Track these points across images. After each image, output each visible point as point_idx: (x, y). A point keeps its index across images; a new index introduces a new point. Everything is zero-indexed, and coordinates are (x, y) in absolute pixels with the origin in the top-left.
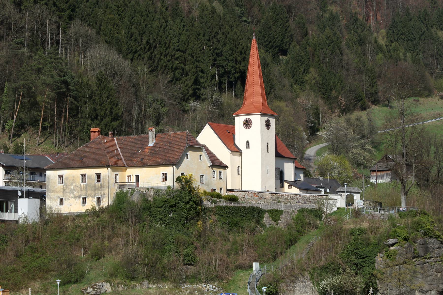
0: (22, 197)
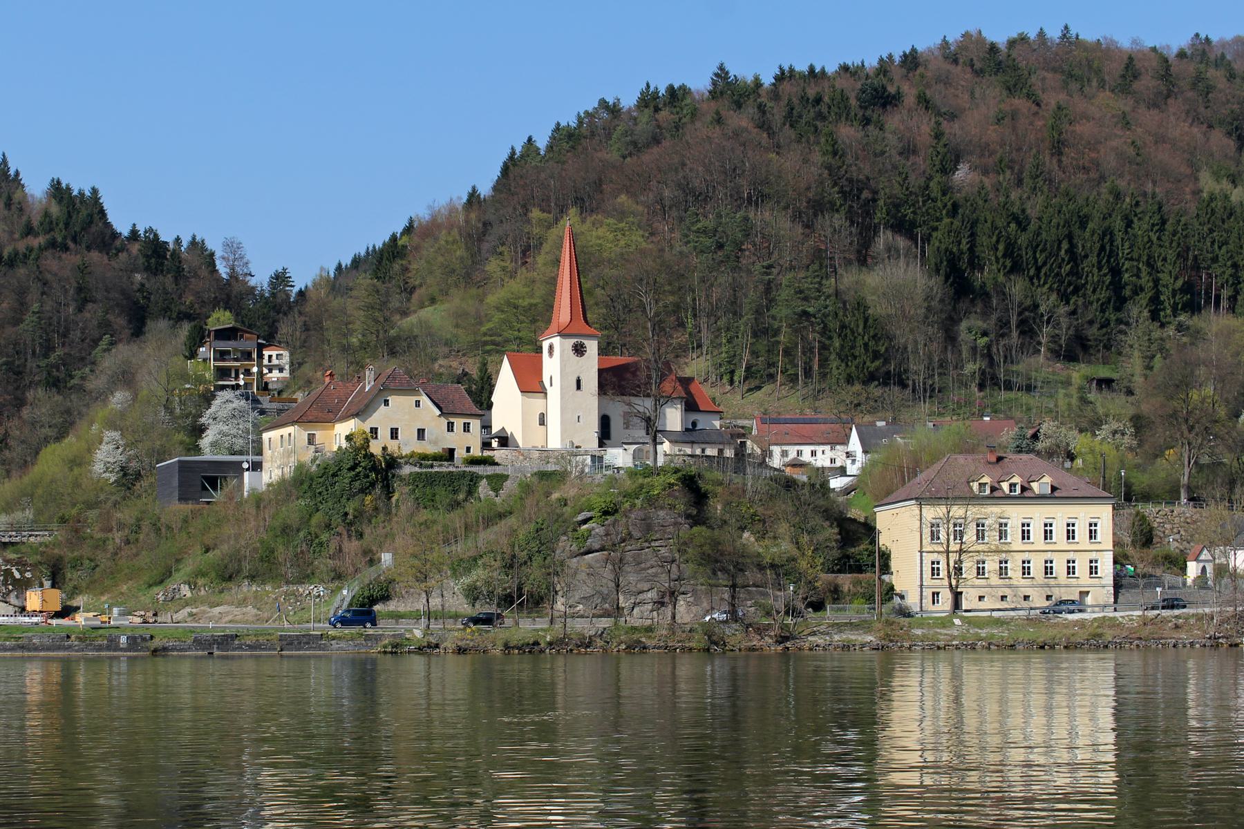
0: (248, 469)
